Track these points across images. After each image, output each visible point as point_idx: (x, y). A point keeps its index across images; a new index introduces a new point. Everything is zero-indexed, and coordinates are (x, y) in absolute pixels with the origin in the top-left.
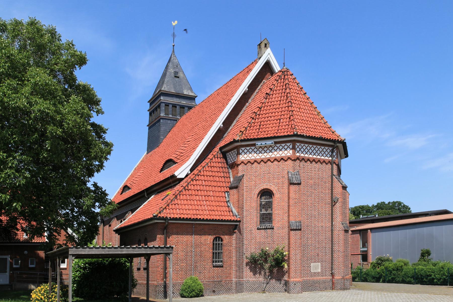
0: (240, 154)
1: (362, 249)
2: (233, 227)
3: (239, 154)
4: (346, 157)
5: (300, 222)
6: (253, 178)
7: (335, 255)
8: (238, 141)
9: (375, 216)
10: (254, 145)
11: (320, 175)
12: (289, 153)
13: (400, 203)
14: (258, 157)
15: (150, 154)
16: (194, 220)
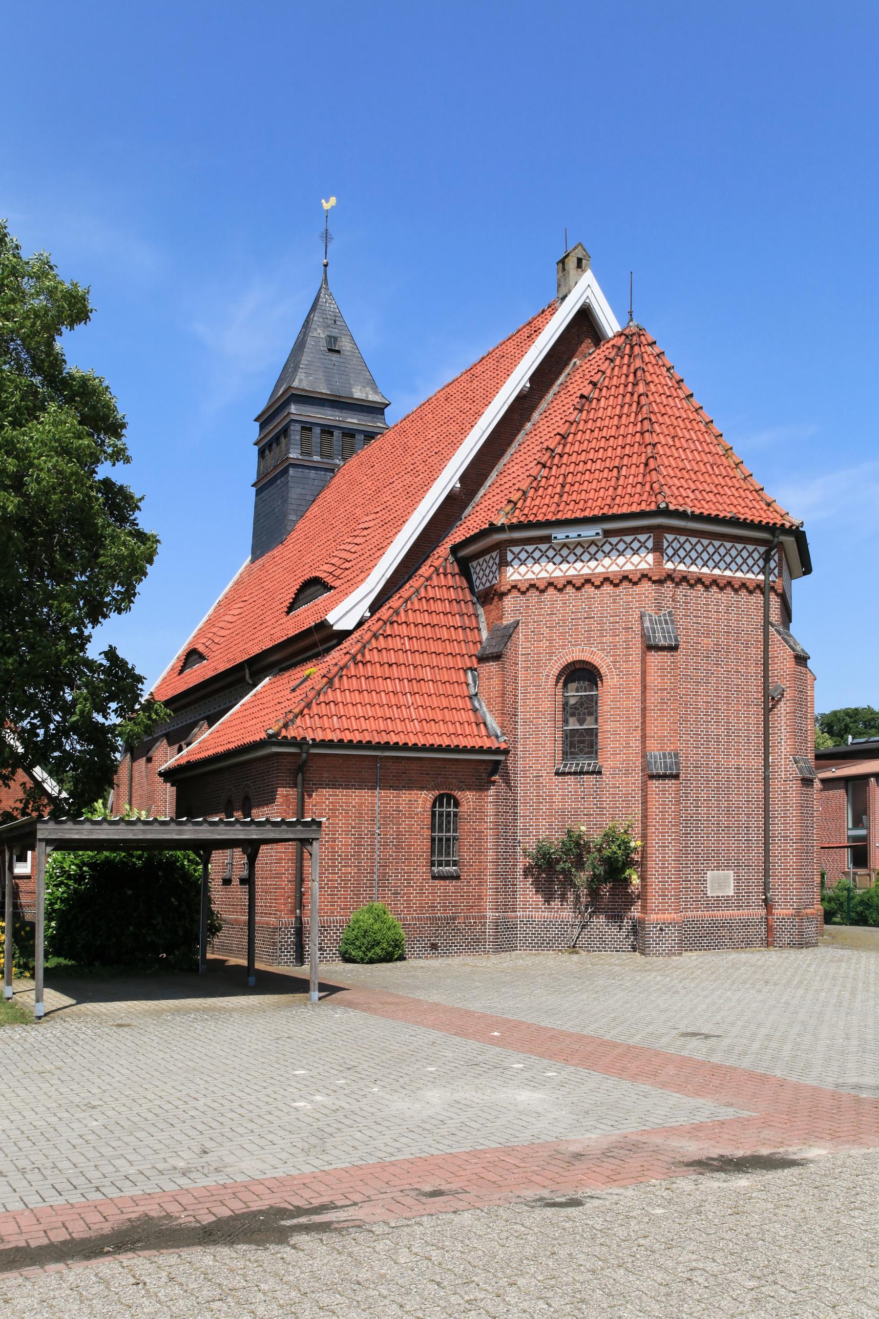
2: (488, 768)
4: (805, 574)
5: (676, 755)
8: (502, 529)
10: (547, 539)
11: (733, 623)
12: (644, 561)
14: (557, 573)
15: (260, 562)
16: (379, 746)
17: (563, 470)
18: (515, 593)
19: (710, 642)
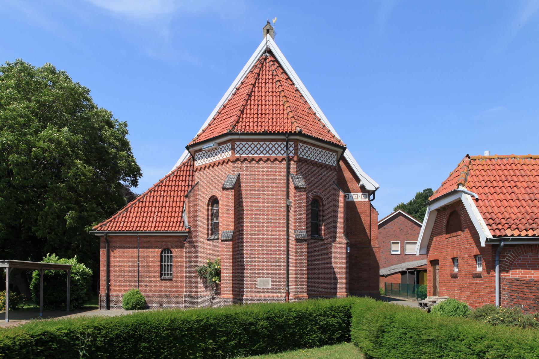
0: (196, 160)
2: (185, 239)
10: (201, 150)
11: (271, 175)
12: (227, 155)
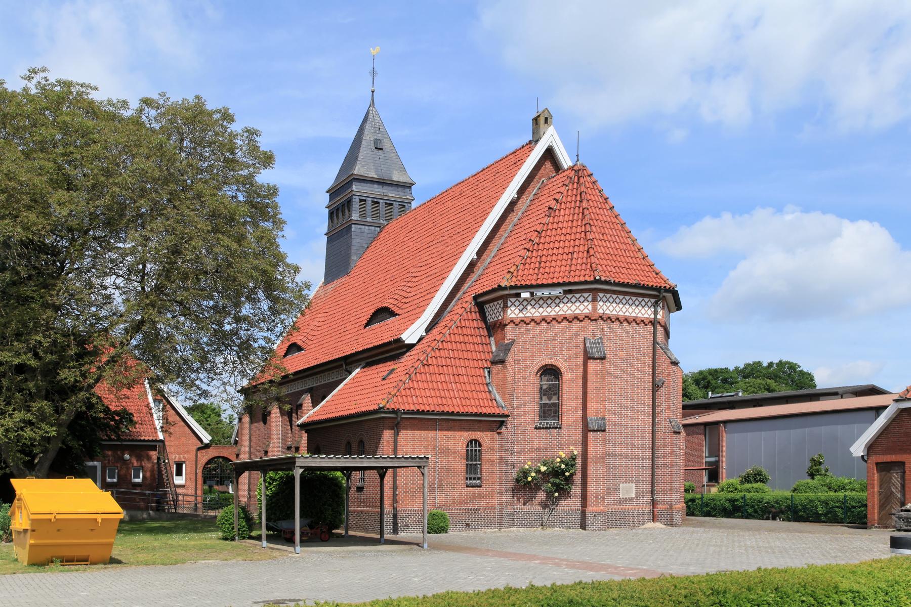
1: (708, 459)
2: (496, 423)
3: (505, 307)
4: (678, 310)
5: (604, 419)
6: (529, 346)
7: (658, 472)
8: (505, 288)
9: (737, 394)
11: (636, 343)
13: (793, 367)
14: (537, 314)
15: (332, 286)
16: (438, 413)
17: (540, 253)
18: (512, 325)
19: (623, 354)
